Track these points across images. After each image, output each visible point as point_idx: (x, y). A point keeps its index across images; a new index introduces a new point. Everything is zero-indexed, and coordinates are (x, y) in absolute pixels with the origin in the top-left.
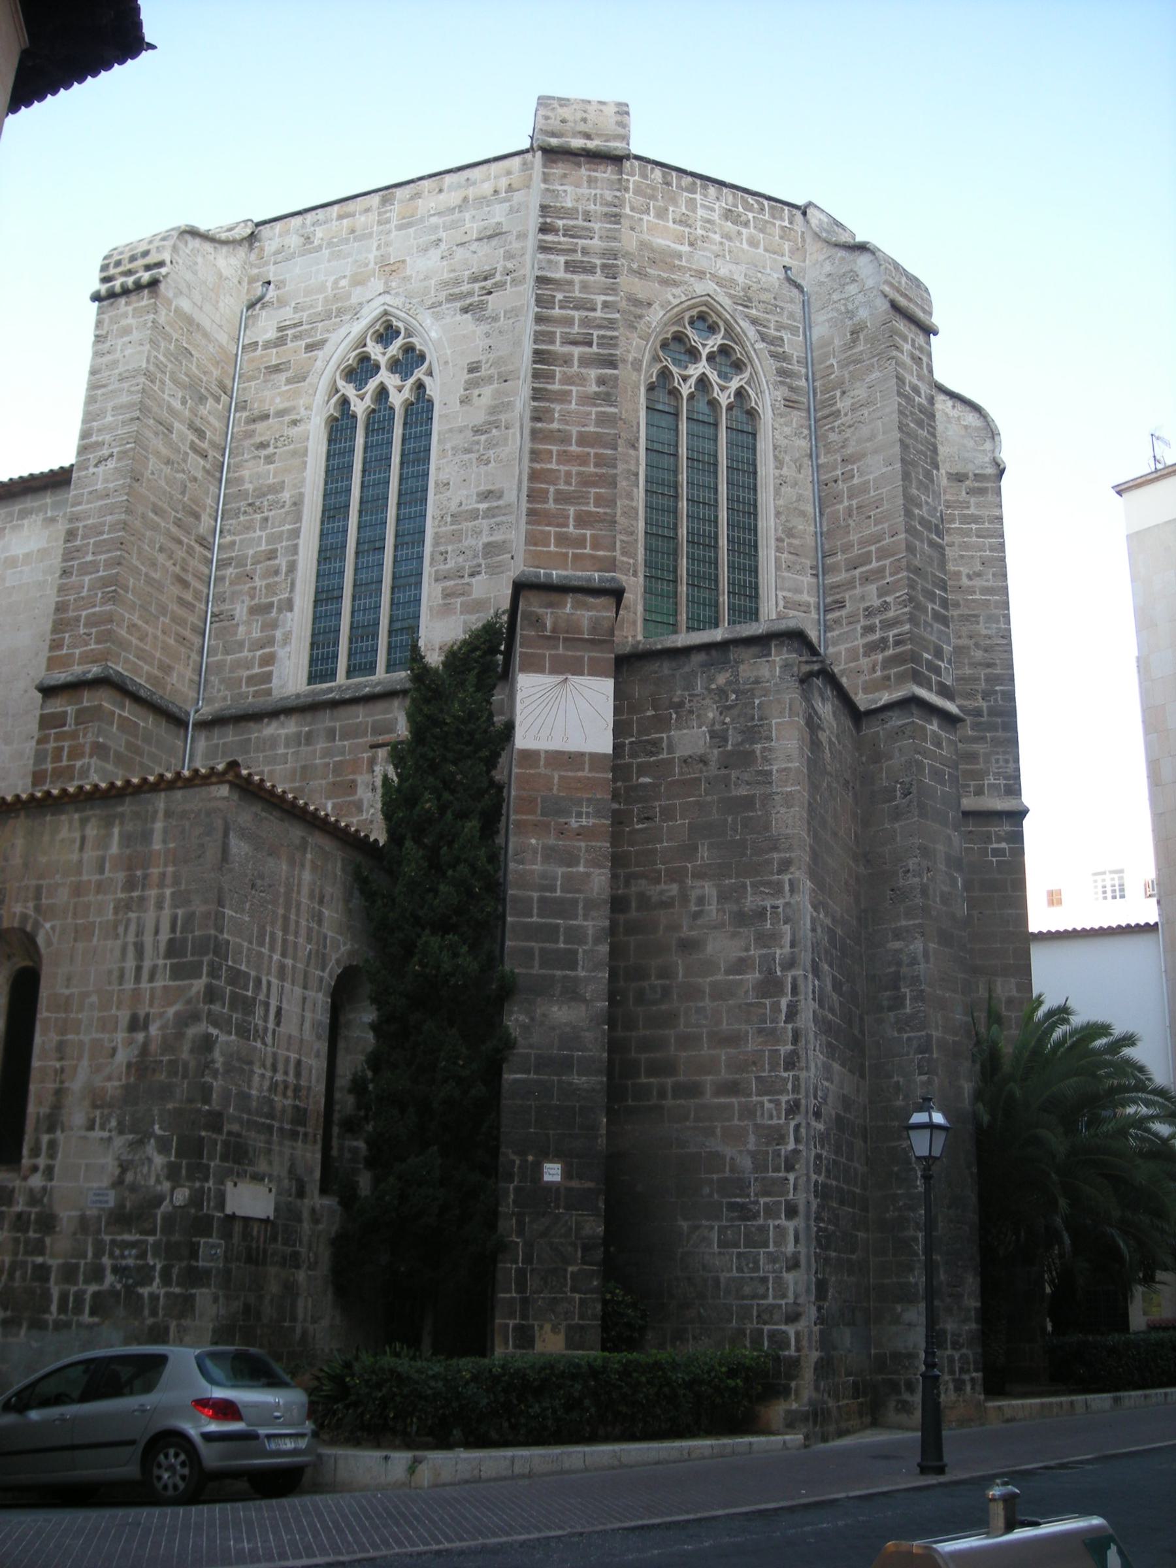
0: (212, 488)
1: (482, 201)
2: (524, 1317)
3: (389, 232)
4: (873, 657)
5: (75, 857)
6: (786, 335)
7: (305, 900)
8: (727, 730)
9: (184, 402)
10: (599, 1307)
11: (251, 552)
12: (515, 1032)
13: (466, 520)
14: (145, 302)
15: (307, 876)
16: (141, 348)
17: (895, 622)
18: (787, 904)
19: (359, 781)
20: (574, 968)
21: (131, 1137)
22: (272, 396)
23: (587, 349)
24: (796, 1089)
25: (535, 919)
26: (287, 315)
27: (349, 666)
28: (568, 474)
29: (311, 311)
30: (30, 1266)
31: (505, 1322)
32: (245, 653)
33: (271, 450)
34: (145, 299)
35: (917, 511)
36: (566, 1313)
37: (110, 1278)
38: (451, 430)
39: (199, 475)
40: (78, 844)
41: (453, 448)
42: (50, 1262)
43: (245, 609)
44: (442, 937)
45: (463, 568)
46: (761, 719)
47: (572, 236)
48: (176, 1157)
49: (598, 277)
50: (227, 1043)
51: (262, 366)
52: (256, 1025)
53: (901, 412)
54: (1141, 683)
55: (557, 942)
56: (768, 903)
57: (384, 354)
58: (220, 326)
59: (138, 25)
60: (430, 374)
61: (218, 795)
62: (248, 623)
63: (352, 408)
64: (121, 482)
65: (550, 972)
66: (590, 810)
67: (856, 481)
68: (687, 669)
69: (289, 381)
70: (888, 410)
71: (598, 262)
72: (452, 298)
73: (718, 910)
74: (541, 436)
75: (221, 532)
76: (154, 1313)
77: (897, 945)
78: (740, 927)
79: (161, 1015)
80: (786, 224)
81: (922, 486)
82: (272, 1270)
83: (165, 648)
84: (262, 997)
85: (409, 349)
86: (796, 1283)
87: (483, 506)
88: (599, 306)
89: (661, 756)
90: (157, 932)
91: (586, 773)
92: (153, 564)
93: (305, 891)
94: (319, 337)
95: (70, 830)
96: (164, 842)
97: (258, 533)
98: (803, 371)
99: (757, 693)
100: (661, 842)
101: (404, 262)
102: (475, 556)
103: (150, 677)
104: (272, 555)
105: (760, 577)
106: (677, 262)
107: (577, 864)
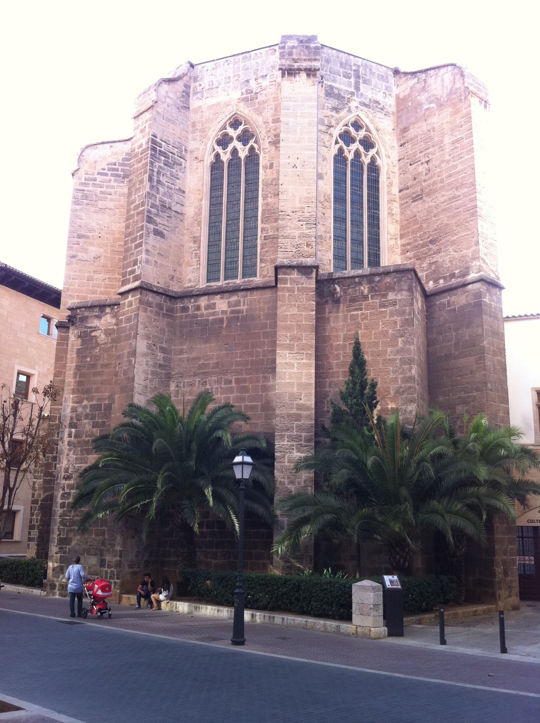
54: (32, 297)
57: (235, 133)
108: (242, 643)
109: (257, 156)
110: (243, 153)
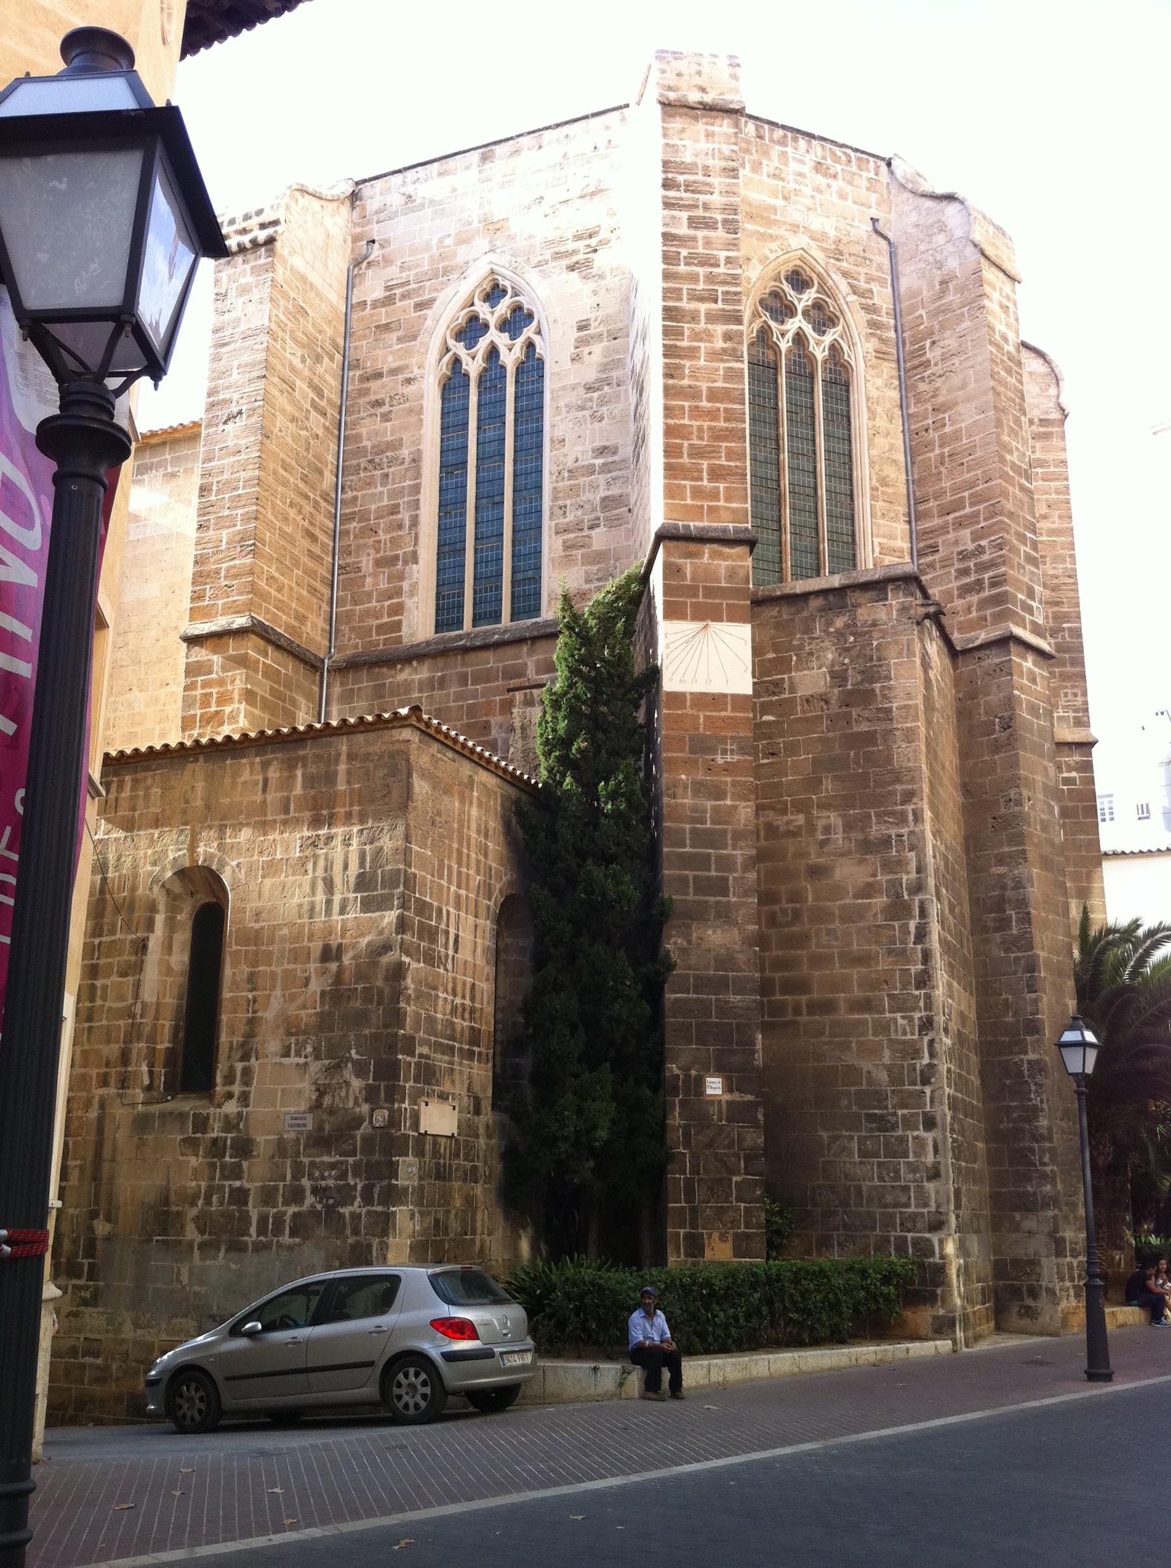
0: (332, 445)
2: (694, 1226)
4: (968, 599)
5: (259, 798)
6: (875, 287)
7: (474, 835)
8: (847, 670)
9: (303, 361)
10: (763, 1216)
11: (373, 507)
12: (674, 957)
13: (583, 475)
14: (262, 261)
15: (474, 812)
16: (262, 306)
18: (911, 833)
19: (493, 723)
22: (385, 356)
23: (713, 306)
24: (929, 1006)
25: (688, 849)
26: (393, 273)
27: (475, 614)
28: (700, 429)
30: (227, 1190)
31: (677, 1232)
32: (374, 604)
33: (386, 408)
34: (262, 258)
35: (1008, 457)
36: (732, 1222)
37: (310, 1200)
38: (564, 388)
39: (320, 432)
40: (260, 785)
41: (566, 406)
42: (247, 1185)
43: (371, 562)
44: (607, 867)
45: (582, 521)
46: (879, 659)
47: (693, 192)
49: (720, 234)
50: (417, 969)
52: (439, 952)
55: (709, 870)
56: (893, 832)
57: (493, 313)
58: (330, 285)
60: (539, 332)
62: (375, 575)
63: (464, 366)
64: (253, 439)
65: (704, 898)
67: (947, 429)
68: (805, 614)
69: (400, 340)
70: (980, 359)
71: (719, 217)
72: (558, 256)
73: (844, 838)
75: (343, 488)
76: (356, 1232)
77: (1001, 870)
78: (866, 854)
80: (872, 175)
82: (457, 1185)
83: (300, 599)
84: (443, 926)
85: (517, 309)
87: (599, 461)
88: (722, 262)
90: (346, 867)
91: (728, 713)
92: (286, 519)
93: (474, 826)
94: (427, 297)
95: (251, 773)
96: (349, 782)
97: (380, 489)
99: (875, 635)
100: (786, 775)
102: (593, 510)
103: (288, 627)
104: (394, 510)
105: (856, 525)
106: (773, 217)
107: (724, 798)
108: (1108, 1378)
109: (541, 362)
110: (510, 358)
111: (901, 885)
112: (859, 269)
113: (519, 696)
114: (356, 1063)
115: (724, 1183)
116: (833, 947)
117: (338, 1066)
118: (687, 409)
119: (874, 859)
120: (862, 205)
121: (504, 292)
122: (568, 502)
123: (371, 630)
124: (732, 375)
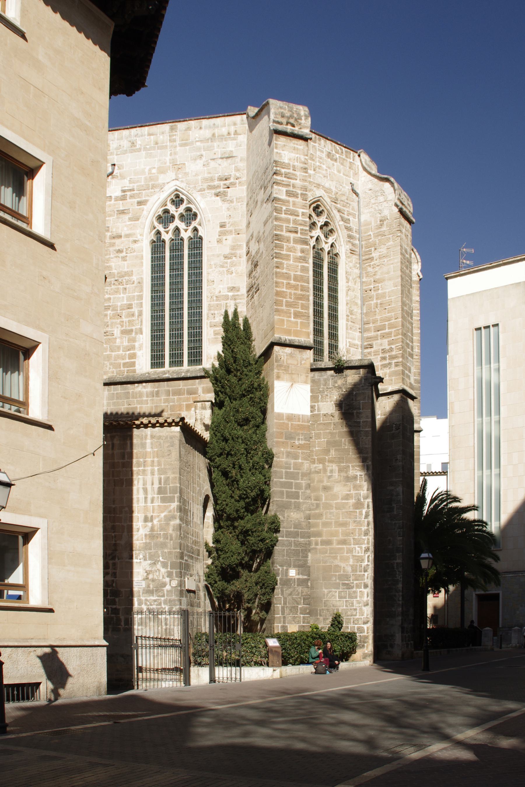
1: (222, 137)
3: (176, 147)
11: (119, 304)
13: (223, 300)
17: (395, 357)
20: (298, 498)
21: (150, 562)
25: (284, 480)
26: (126, 184)
28: (290, 294)
29: (138, 184)
32: (121, 352)
33: (124, 254)
35: (405, 308)
38: (213, 255)
41: (215, 264)
42: (118, 607)
47: (288, 178)
48: (171, 569)
51: (115, 210)
53: (401, 262)
57: (177, 211)
59: (145, 79)
61: (175, 430)
62: (121, 338)
65: (290, 500)
66: (303, 437)
67: (380, 291)
69: (130, 219)
71: (299, 192)
72: (210, 187)
73: (338, 475)
74: (279, 275)
79: (158, 516)
80: (351, 161)
81: (407, 296)
85: (189, 210)
86: (367, 611)
87: (230, 294)
88: (300, 215)
89: (315, 413)
90: (153, 484)
94: (144, 199)
96: (152, 448)
97: (122, 295)
98: (358, 236)
101: (184, 164)
104: (130, 307)
107: (298, 459)
110: (186, 235)
111: (360, 495)
112: (344, 208)
113: (199, 404)
114: (162, 562)
115: (296, 608)
116: (332, 519)
117: (154, 563)
118: (285, 284)
119: (350, 485)
120: (347, 176)
121: (182, 201)
122: (216, 312)
123: (120, 365)
124: (305, 269)
